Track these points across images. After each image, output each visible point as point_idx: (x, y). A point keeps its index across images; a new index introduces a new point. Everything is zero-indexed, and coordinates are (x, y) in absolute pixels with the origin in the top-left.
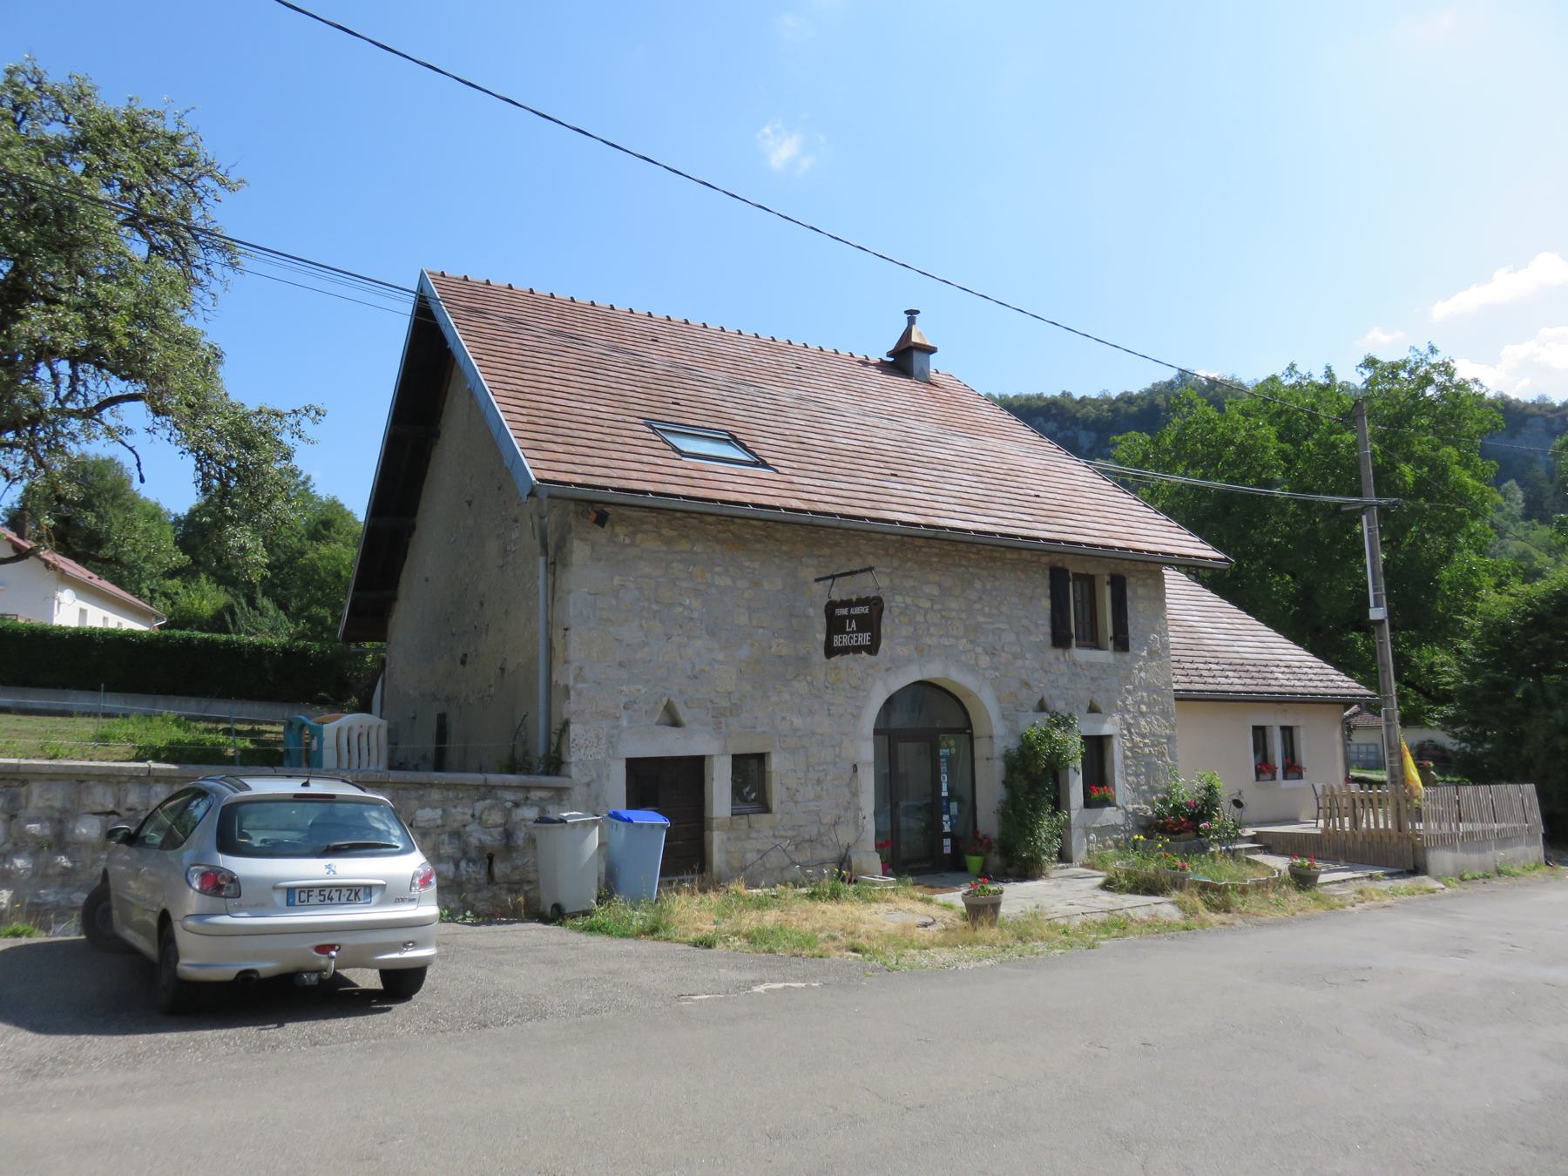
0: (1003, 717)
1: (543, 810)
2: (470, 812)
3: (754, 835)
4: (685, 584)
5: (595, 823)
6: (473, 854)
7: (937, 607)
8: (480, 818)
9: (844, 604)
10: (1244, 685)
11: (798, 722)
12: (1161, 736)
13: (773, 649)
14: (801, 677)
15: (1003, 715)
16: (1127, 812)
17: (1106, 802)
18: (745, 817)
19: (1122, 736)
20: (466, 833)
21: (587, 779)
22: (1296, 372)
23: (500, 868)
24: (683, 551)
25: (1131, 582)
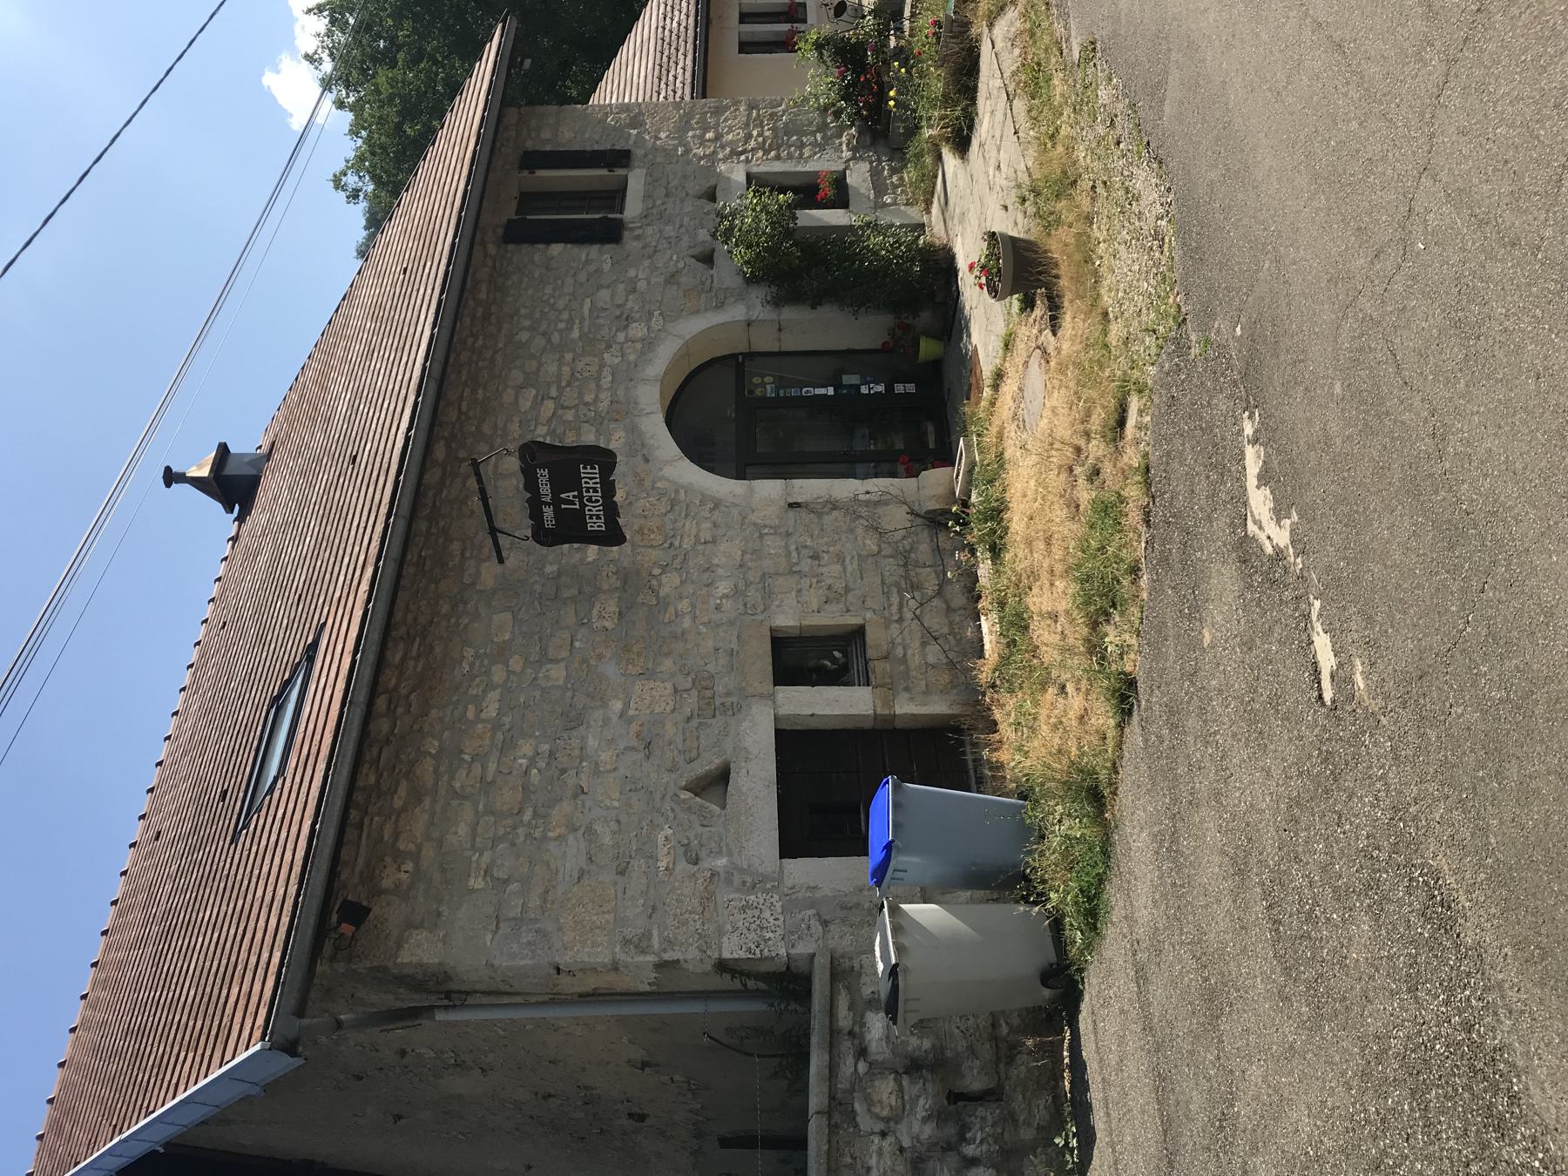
0: (720, 306)
1: (872, 1003)
2: (876, 1140)
3: (899, 651)
4: (492, 767)
5: (894, 910)
6: (951, 1130)
7: (554, 392)
8: (887, 1120)
9: (536, 514)
10: (685, 56)
11: (723, 588)
12: (749, 115)
13: (608, 624)
14: (654, 582)
15: (717, 307)
16: (853, 158)
17: (840, 181)
18: (871, 664)
19: (747, 161)
20: (913, 1147)
21: (816, 926)
22: (316, 53)
23: (974, 1080)
24: (436, 771)
25: (530, 145)
